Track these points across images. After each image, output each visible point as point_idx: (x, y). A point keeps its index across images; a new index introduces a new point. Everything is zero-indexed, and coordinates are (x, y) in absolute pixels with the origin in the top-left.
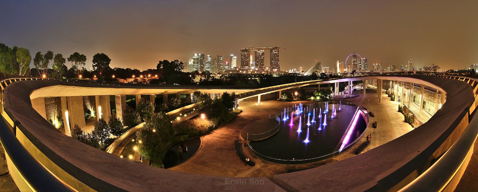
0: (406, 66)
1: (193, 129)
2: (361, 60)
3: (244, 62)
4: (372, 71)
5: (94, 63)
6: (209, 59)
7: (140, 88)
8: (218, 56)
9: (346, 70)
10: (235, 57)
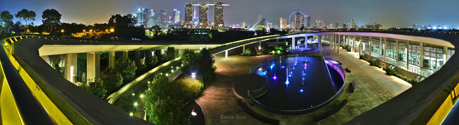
1: (186, 92)
3: (188, 18)
4: (315, 27)
5: (44, 19)
6: (153, 14)
7: (119, 45)
8: (161, 11)
9: (289, 26)
10: (179, 12)
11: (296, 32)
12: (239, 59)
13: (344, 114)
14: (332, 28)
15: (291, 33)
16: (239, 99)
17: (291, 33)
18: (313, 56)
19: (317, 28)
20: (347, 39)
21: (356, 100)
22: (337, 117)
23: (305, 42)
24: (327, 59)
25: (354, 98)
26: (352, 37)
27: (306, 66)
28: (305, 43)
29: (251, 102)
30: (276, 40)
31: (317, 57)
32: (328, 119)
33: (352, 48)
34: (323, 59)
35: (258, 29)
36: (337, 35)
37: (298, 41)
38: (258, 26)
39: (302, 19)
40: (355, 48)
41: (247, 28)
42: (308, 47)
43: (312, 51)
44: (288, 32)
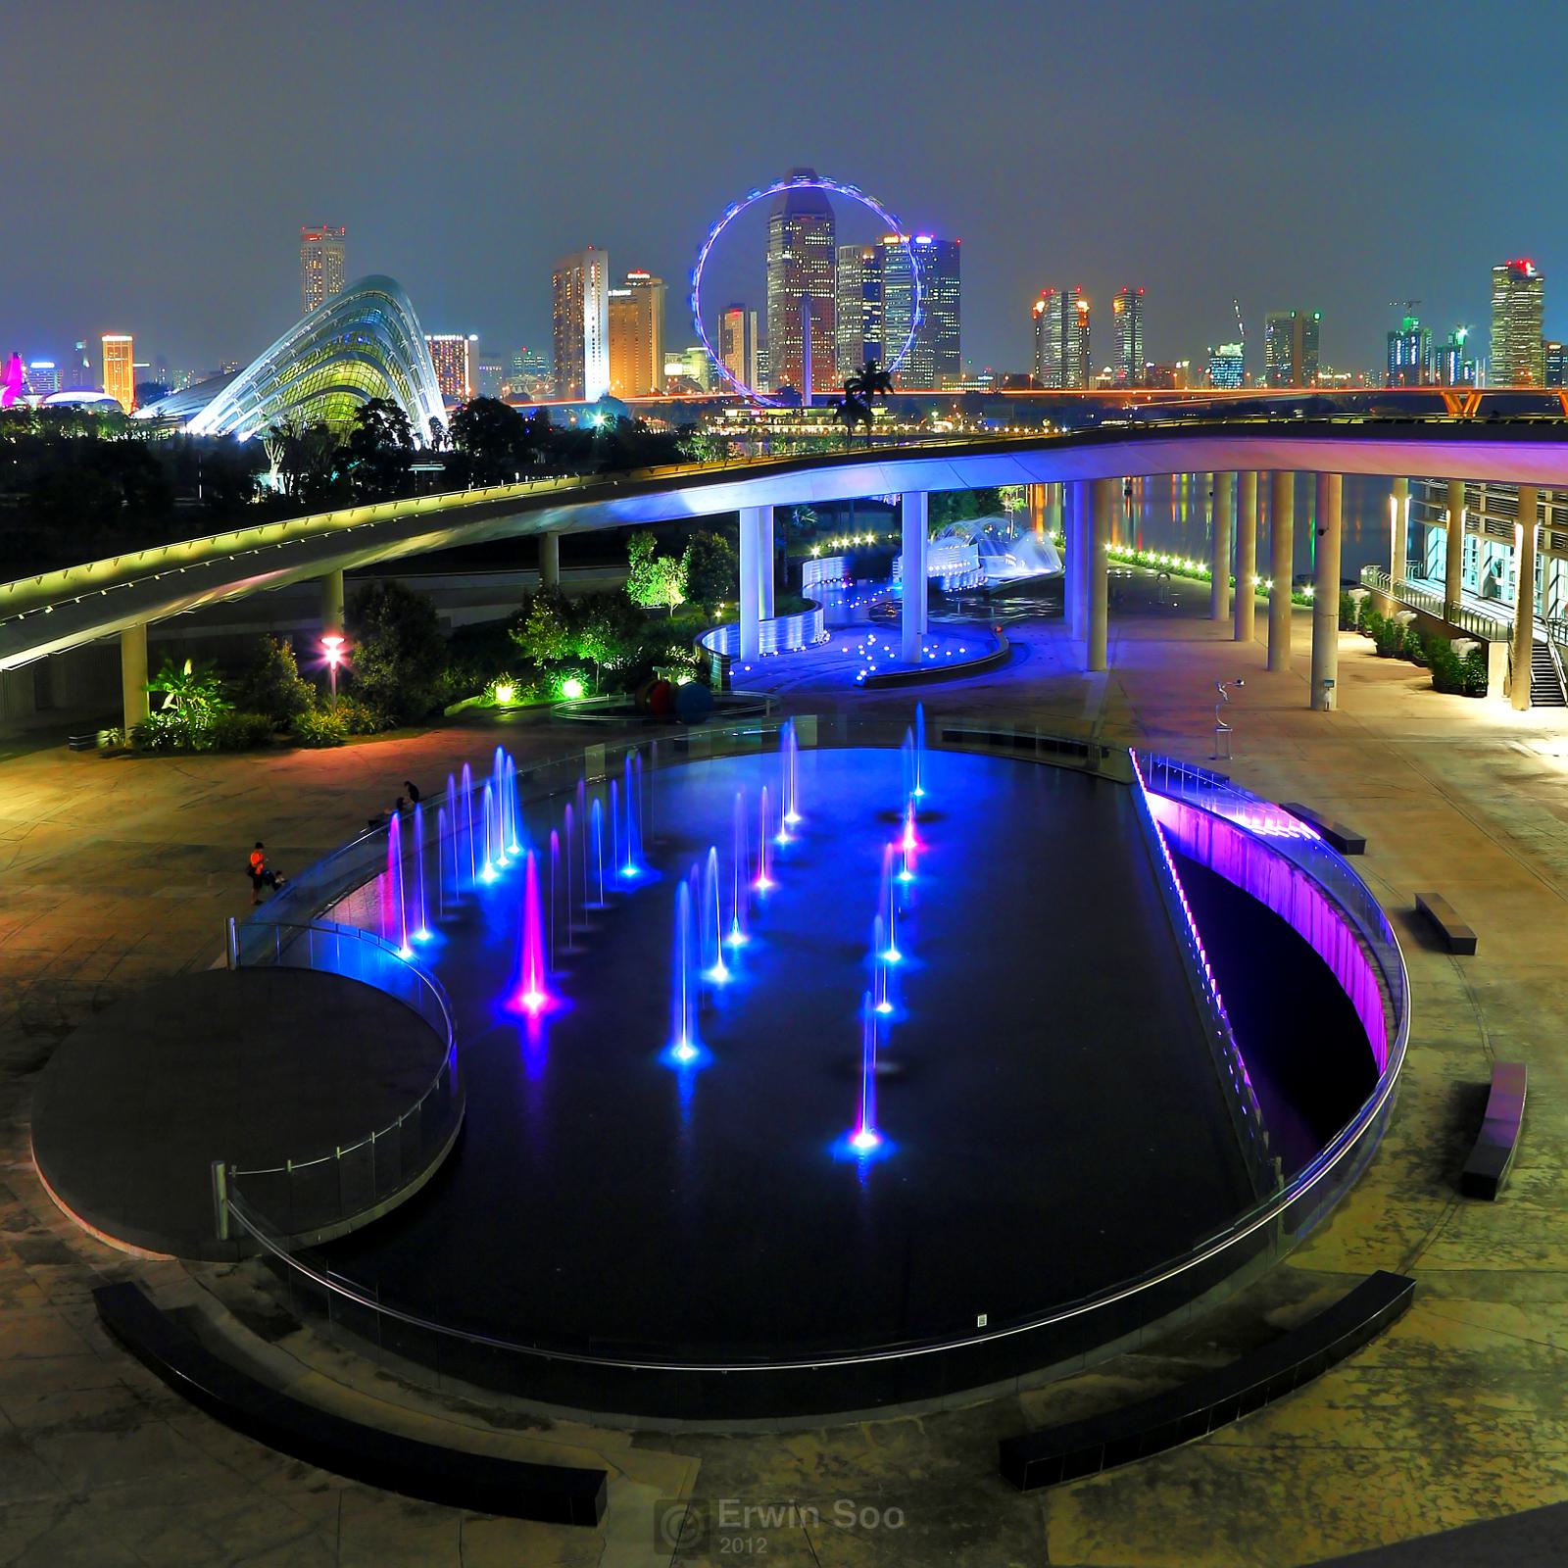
0: (1462, 334)
2: (881, 251)
4: (1020, 381)
11: (789, 439)
12: (85, 798)
13: (1360, 1434)
14: (1233, 390)
15: (724, 453)
16: (111, 1275)
17: (724, 453)
18: (996, 740)
19: (1052, 388)
20: (1437, 538)
21: (1518, 1293)
22: (1276, 1459)
23: (900, 566)
24: (1175, 777)
25: (1498, 1263)
26: (1503, 510)
27: (917, 854)
28: (898, 586)
29: (264, 1298)
30: (525, 551)
31: (1049, 746)
32: (1165, 1468)
33: (1499, 655)
34: (1120, 775)
35: (295, 414)
36: (1302, 475)
37: (816, 551)
38: (302, 380)
39: (862, 276)
40: (1541, 648)
41: (170, 408)
42: (937, 632)
43: (979, 680)
44: (686, 439)
